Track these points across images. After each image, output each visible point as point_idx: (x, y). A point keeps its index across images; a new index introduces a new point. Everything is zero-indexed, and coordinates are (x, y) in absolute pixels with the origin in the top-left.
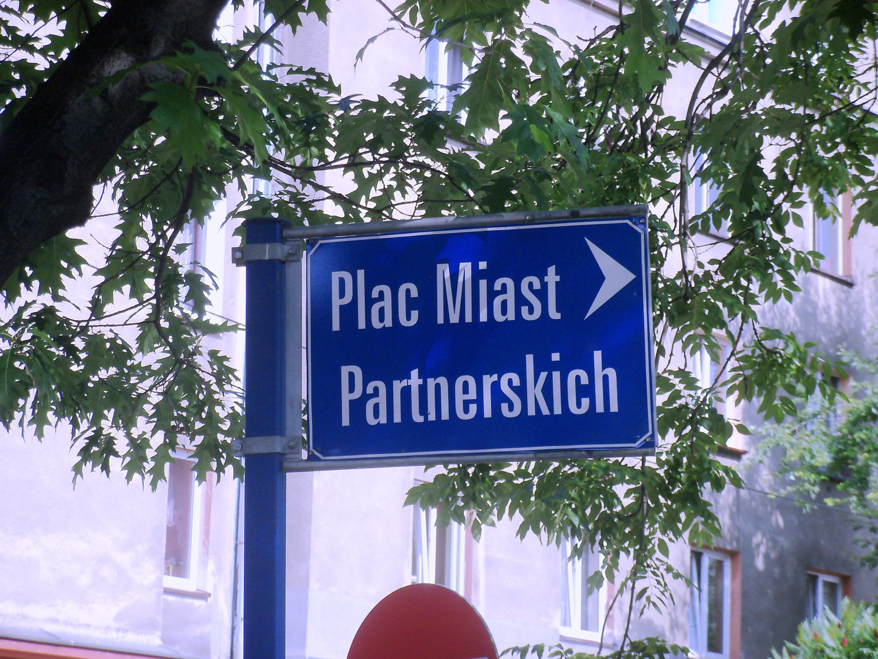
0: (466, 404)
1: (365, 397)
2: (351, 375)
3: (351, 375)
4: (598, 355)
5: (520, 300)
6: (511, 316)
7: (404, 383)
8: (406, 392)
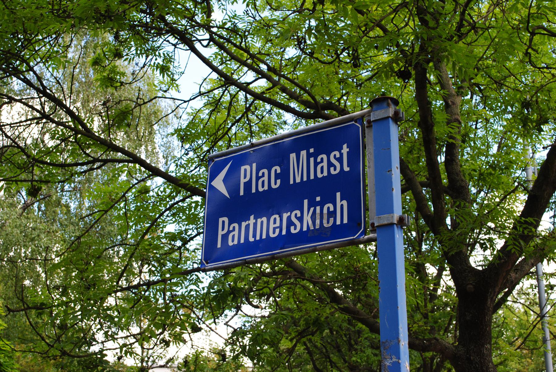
0: (274, 229)
1: (229, 232)
2: (223, 222)
3: (223, 222)
4: (338, 195)
5: (330, 164)
6: (325, 174)
7: (247, 223)
8: (247, 227)
